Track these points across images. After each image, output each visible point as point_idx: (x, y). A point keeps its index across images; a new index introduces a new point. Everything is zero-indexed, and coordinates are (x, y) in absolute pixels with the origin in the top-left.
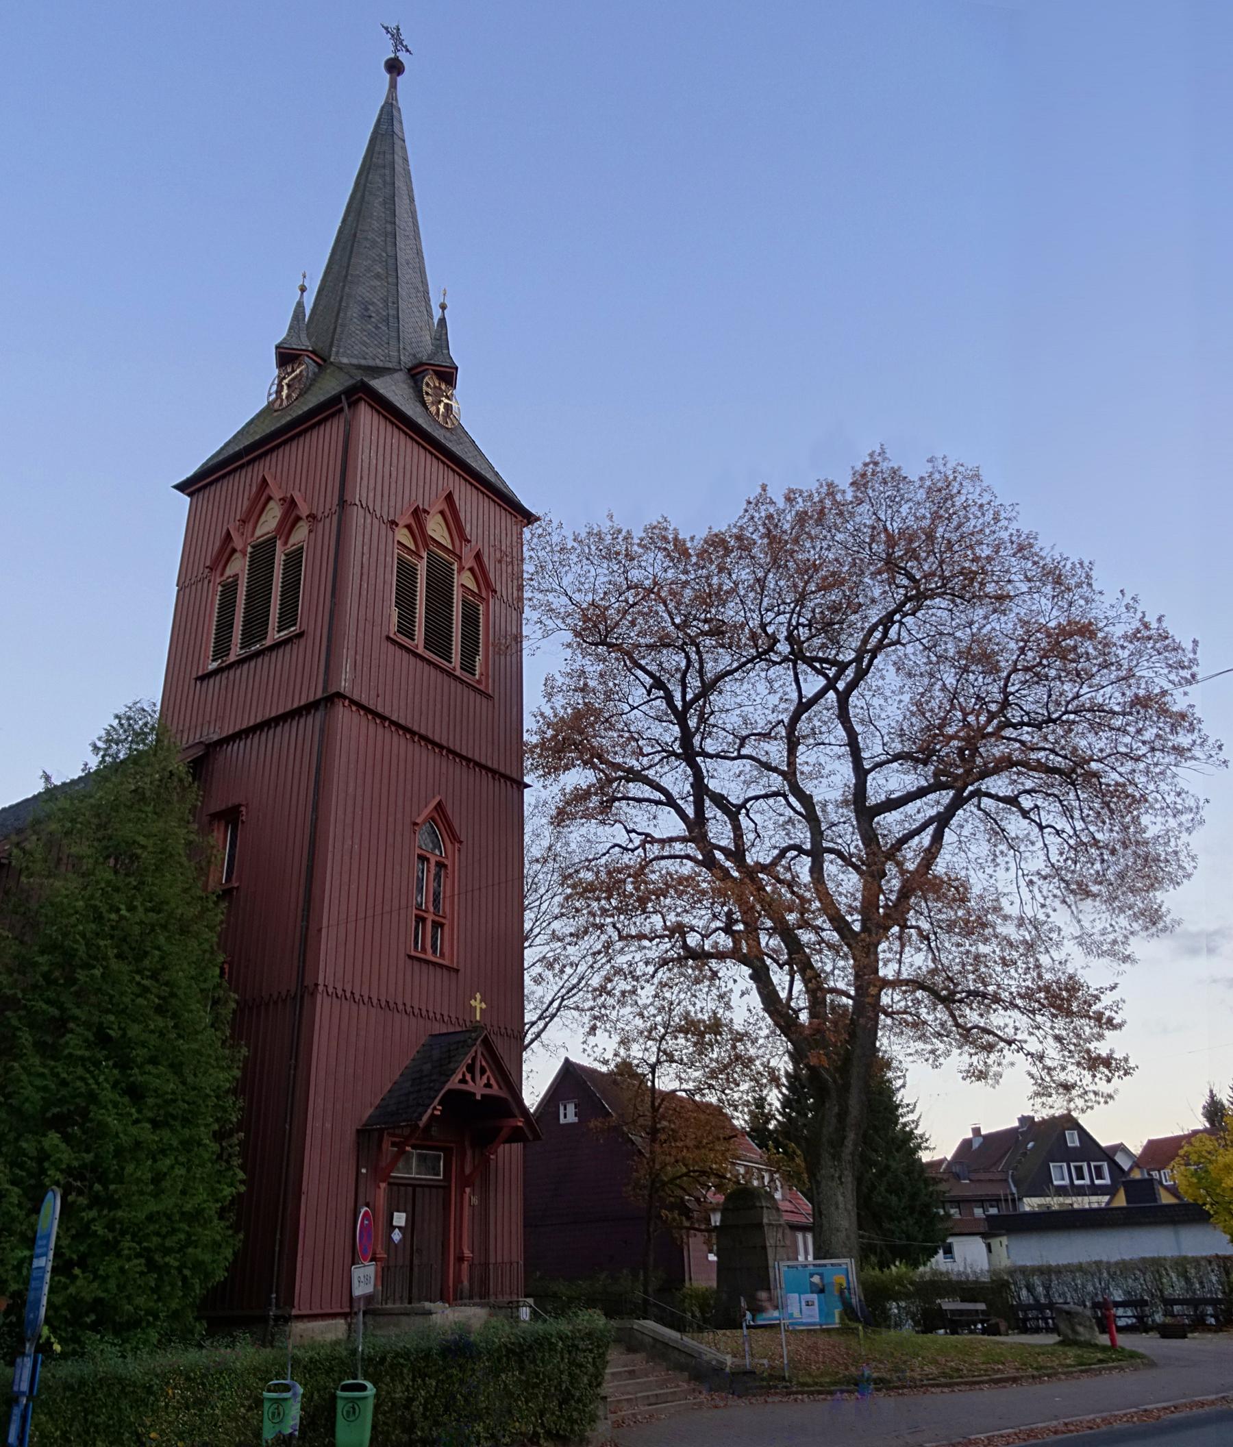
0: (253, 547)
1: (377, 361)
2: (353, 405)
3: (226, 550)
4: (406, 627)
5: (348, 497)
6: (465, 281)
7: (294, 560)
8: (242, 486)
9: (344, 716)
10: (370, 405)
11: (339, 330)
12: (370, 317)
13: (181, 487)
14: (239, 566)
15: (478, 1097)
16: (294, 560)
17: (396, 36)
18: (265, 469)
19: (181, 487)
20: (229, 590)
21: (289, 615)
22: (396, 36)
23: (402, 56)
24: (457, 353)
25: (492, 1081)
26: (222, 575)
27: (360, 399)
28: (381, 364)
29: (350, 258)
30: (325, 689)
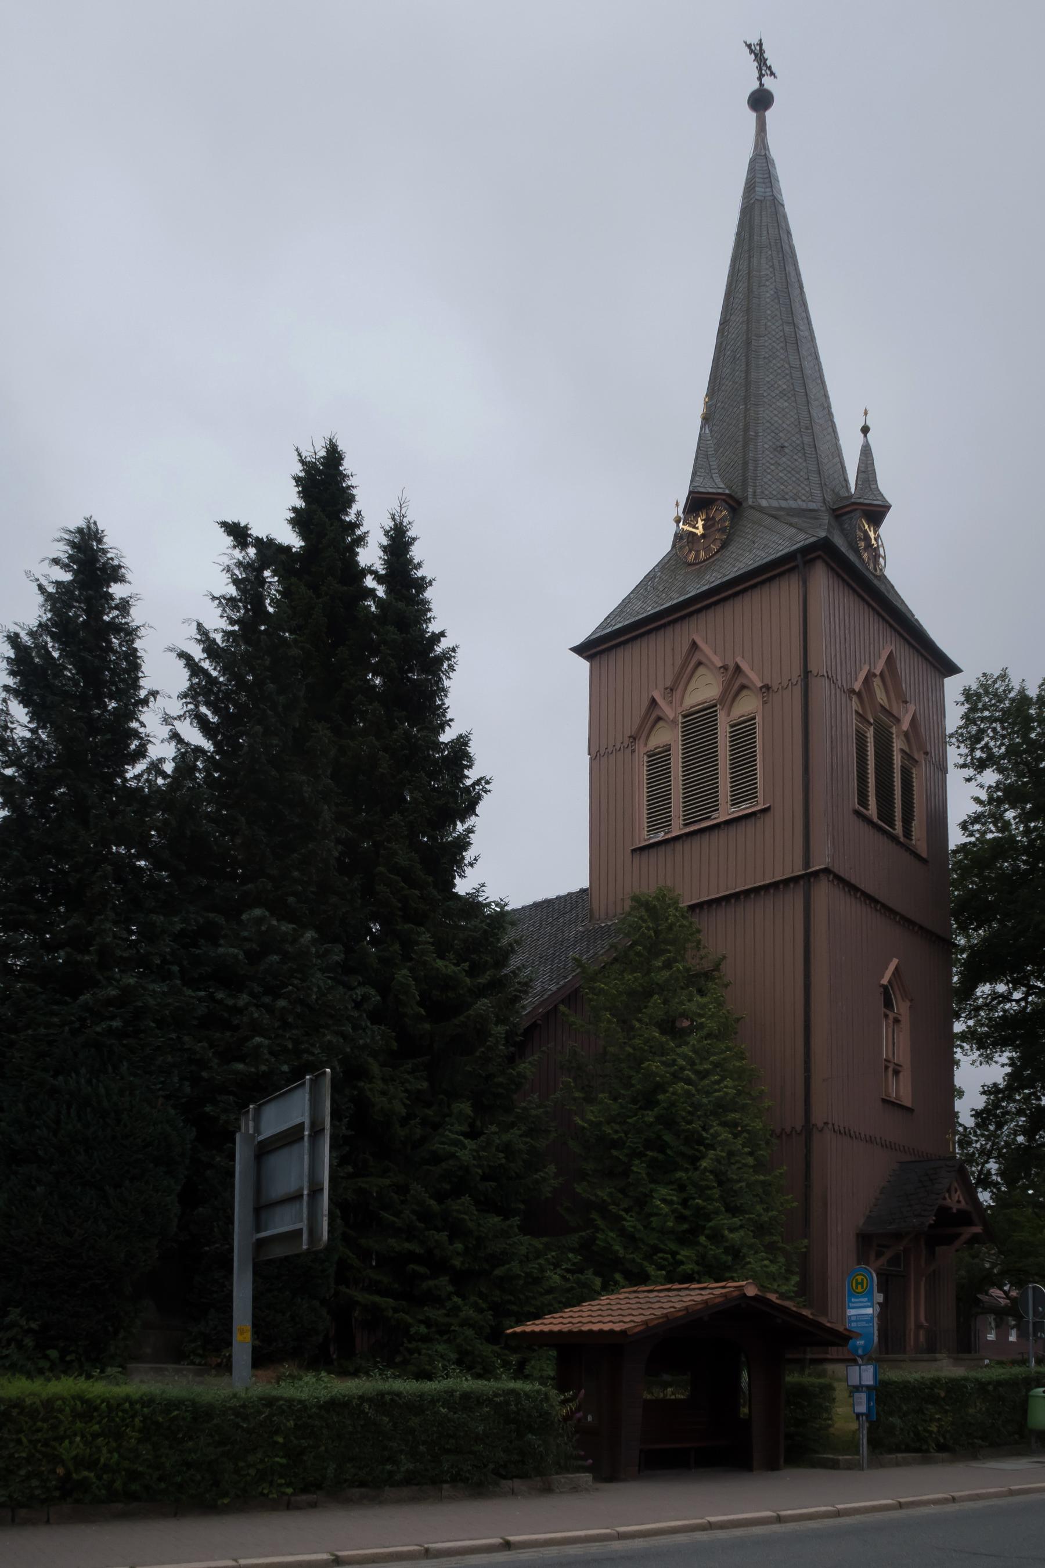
0: (685, 716)
1: (799, 502)
2: (809, 563)
3: (652, 716)
4: (863, 800)
5: (813, 667)
6: (878, 391)
7: (743, 733)
8: (660, 654)
9: (823, 892)
10: (828, 565)
11: (751, 467)
12: (783, 447)
13: (580, 650)
14: (668, 737)
15: (955, 1211)
16: (743, 733)
17: (758, 53)
18: (700, 631)
19: (580, 650)
20: (659, 760)
21: (743, 791)
22: (758, 53)
23: (768, 82)
24: (887, 485)
25: (961, 1199)
26: (646, 745)
27: (819, 557)
28: (804, 506)
29: (747, 372)
30: (807, 864)
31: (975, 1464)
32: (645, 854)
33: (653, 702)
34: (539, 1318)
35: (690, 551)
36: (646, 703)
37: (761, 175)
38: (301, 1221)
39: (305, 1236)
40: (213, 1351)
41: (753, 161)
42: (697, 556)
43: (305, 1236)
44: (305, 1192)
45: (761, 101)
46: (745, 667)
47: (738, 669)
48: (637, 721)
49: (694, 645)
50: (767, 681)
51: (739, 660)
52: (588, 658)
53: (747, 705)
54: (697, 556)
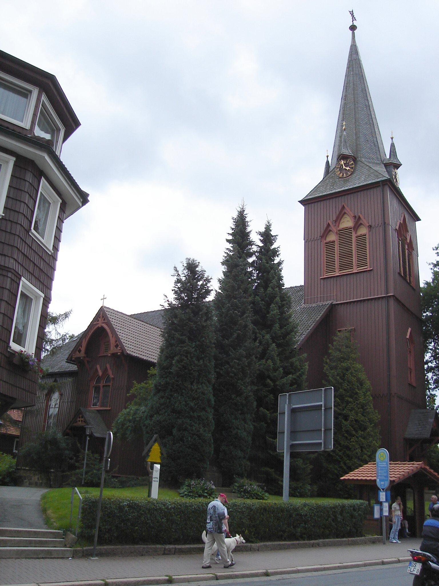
2: (384, 185)
13: (302, 202)
17: (352, 13)
19: (302, 202)
22: (352, 13)
23: (355, 23)
27: (387, 184)
31: (198, 555)
32: (325, 280)
33: (329, 225)
34: (348, 473)
35: (340, 173)
36: (325, 226)
37: (354, 51)
38: (321, 439)
39: (323, 446)
40: (279, 493)
41: (351, 46)
42: (343, 175)
43: (323, 446)
44: (323, 429)
45: (353, 28)
46: (361, 217)
47: (359, 218)
48: (323, 231)
49: (343, 207)
50: (370, 224)
51: (360, 214)
52: (303, 205)
53: (363, 231)
54: (343, 175)
